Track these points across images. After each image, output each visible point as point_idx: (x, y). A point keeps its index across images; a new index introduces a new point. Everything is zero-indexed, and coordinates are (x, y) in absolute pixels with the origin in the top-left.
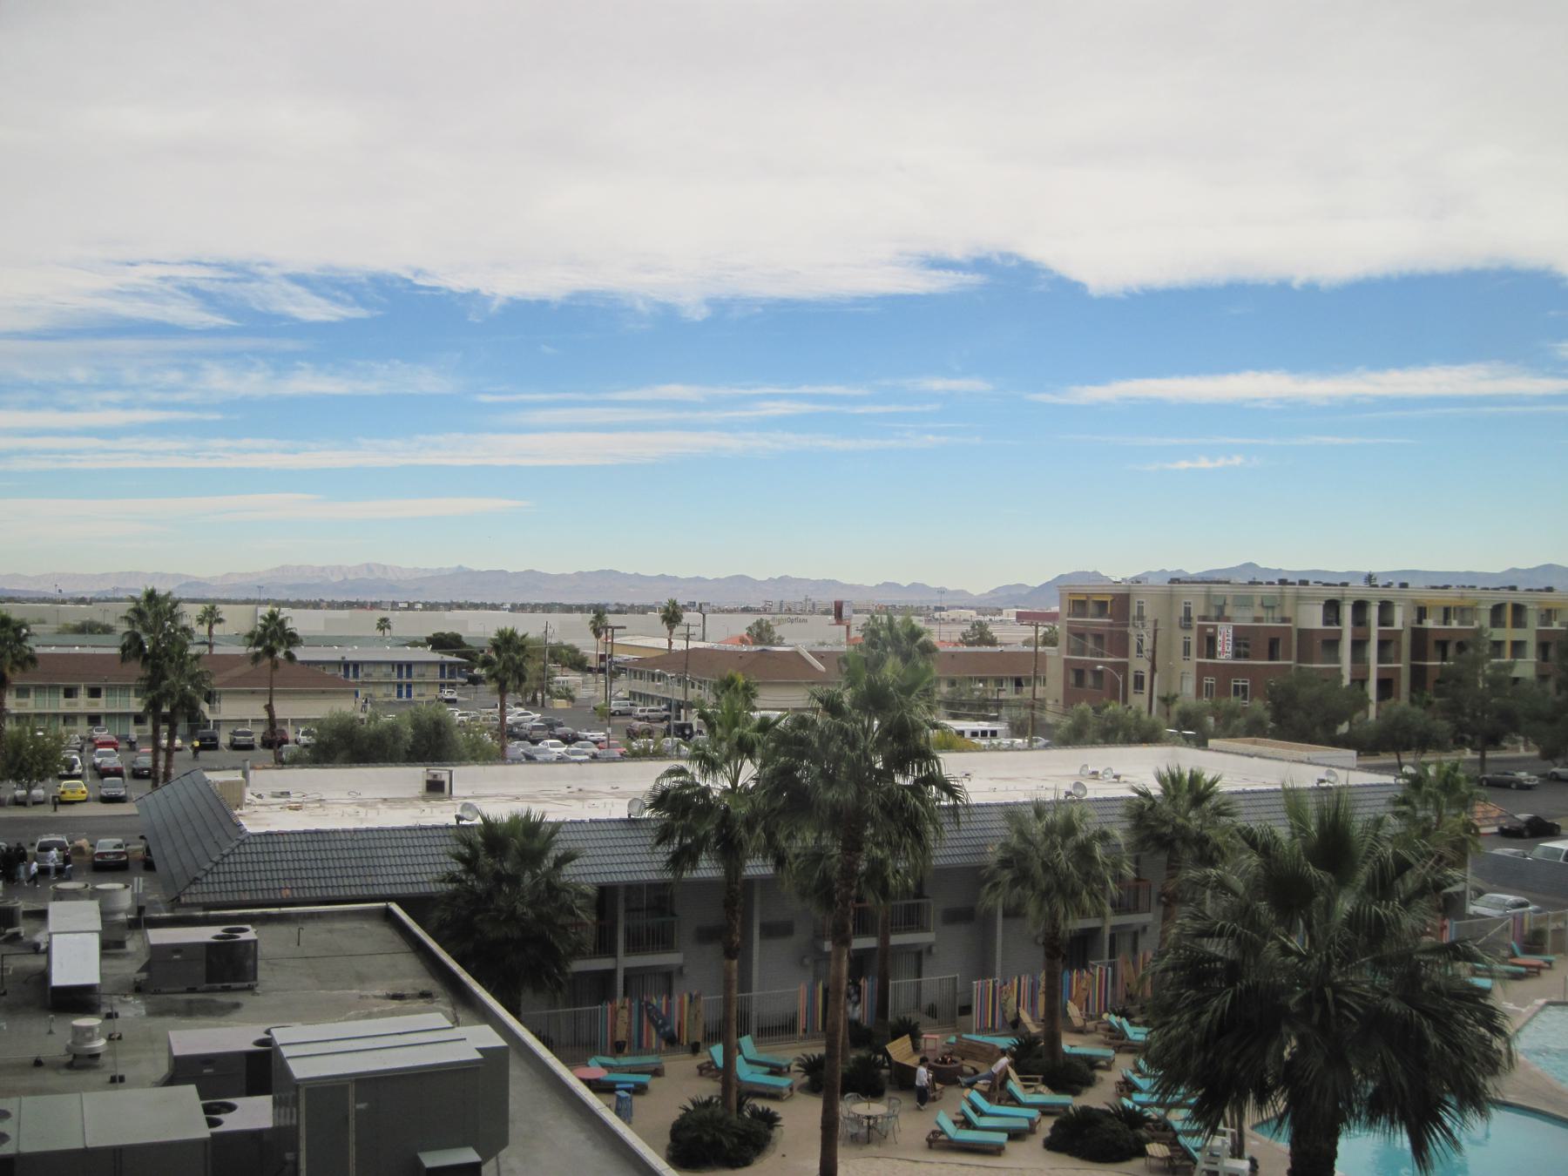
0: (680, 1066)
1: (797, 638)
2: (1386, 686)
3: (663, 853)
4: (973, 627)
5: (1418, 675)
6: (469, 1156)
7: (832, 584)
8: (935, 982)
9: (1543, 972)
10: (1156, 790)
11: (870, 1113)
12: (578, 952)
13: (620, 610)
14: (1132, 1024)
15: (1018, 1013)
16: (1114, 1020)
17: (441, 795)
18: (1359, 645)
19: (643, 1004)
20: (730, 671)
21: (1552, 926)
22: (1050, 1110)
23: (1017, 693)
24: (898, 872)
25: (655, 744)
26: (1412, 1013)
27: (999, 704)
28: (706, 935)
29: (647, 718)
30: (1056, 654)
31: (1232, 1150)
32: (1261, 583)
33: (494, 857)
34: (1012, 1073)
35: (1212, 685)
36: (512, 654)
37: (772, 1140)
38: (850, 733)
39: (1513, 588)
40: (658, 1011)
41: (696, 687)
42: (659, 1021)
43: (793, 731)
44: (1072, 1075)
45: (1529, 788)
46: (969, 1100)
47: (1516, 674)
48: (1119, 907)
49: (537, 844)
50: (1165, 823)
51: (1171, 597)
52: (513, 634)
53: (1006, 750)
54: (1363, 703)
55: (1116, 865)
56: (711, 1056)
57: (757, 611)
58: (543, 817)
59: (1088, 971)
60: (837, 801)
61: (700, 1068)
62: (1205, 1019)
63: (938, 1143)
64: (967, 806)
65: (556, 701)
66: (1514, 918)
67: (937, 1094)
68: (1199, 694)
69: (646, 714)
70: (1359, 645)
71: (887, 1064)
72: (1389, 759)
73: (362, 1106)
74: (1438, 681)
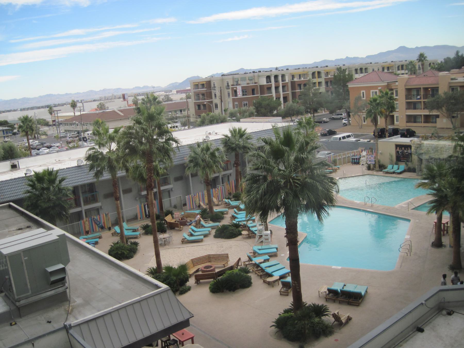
0: (106, 234)
1: (113, 106)
2: (285, 99)
3: (92, 173)
4: (165, 96)
5: (294, 95)
6: (61, 266)
7: (118, 89)
8: (175, 198)
9: (337, 170)
10: (229, 135)
11: (164, 237)
12: (71, 207)
13: (55, 106)
14: (231, 201)
15: (200, 203)
16: (227, 200)
17: (16, 169)
18: (277, 88)
19: (92, 219)
20: (97, 119)
21: (338, 158)
22: (214, 227)
23: (181, 114)
24: (161, 168)
25: (77, 144)
26: (314, 182)
27: (177, 118)
28: (107, 196)
29: (72, 137)
30: (191, 101)
31: (265, 229)
32: (248, 73)
33: (40, 183)
34: (201, 219)
35: (237, 104)
36: (28, 123)
37: (138, 250)
38: (145, 129)
39: (317, 67)
40: (97, 220)
41: (85, 125)
42: (97, 223)
43: (128, 131)
44: (217, 217)
45: (327, 122)
46: (191, 229)
47: (320, 91)
48: (225, 170)
49: (52, 177)
50: (233, 144)
51: (222, 80)
52: (27, 117)
53: (183, 130)
54: (280, 104)
55: (222, 157)
56: (115, 230)
57: (98, 100)
58: (53, 169)
59: (217, 188)
60: (145, 149)
61: (112, 234)
62: (260, 191)
63: (184, 242)
64: (182, 146)
65: (42, 136)
66: (328, 157)
67: (181, 229)
68: (234, 108)
69: (71, 136)
70: (277, 88)
71: (166, 223)
72: (289, 119)
73: (26, 258)
74: (300, 96)
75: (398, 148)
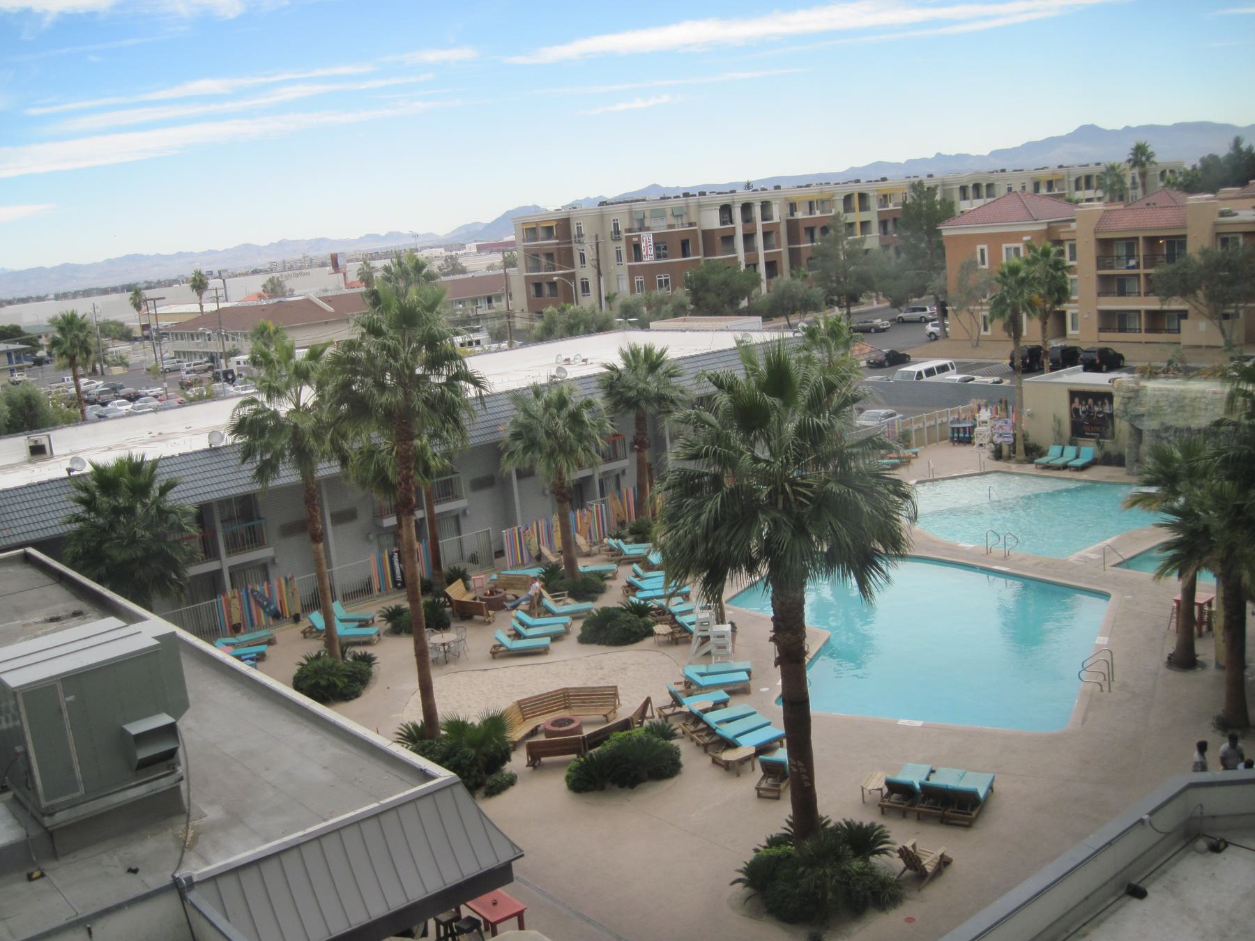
0: (287, 634)
1: (306, 288)
2: (772, 267)
3: (250, 468)
4: (446, 260)
5: (794, 256)
6: (164, 719)
7: (320, 241)
8: (474, 535)
9: (912, 461)
10: (621, 365)
11: (443, 641)
12: (192, 560)
13: (150, 286)
14: (626, 543)
15: (540, 549)
16: (613, 542)
17: (44, 456)
18: (749, 238)
19: (249, 591)
20: (262, 321)
21: (914, 427)
22: (579, 615)
23: (489, 308)
24: (435, 454)
25: (207, 389)
26: (849, 491)
27: (477, 319)
28: (289, 530)
29: (194, 371)
30: (517, 273)
31: (717, 620)
32: (670, 198)
33: (108, 496)
34: (544, 592)
35: (642, 282)
36: (76, 332)
37: (373, 675)
38: (392, 348)
39: (858, 181)
40: (262, 596)
41: (230, 338)
42: (262, 602)
43: (345, 353)
44: (587, 588)
45: (884, 330)
46: (517, 618)
47: (866, 247)
48: (608, 459)
49: (142, 479)
50: (630, 389)
51: (602, 217)
52: (74, 316)
53: (496, 352)
54: (756, 282)
55: (600, 426)
56: (311, 622)
57: (265, 271)
58: (143, 457)
59: (588, 510)
60: (391, 402)
61: (304, 632)
62: (704, 518)
63: (499, 653)
64: (493, 395)
65: (112, 368)
66: (888, 425)
67: (490, 619)
68: (632, 291)
69: (192, 367)
70: (749, 238)
71: (448, 604)
72: (782, 321)
73: (71, 698)
74: (811, 258)
75: (1077, 400)
